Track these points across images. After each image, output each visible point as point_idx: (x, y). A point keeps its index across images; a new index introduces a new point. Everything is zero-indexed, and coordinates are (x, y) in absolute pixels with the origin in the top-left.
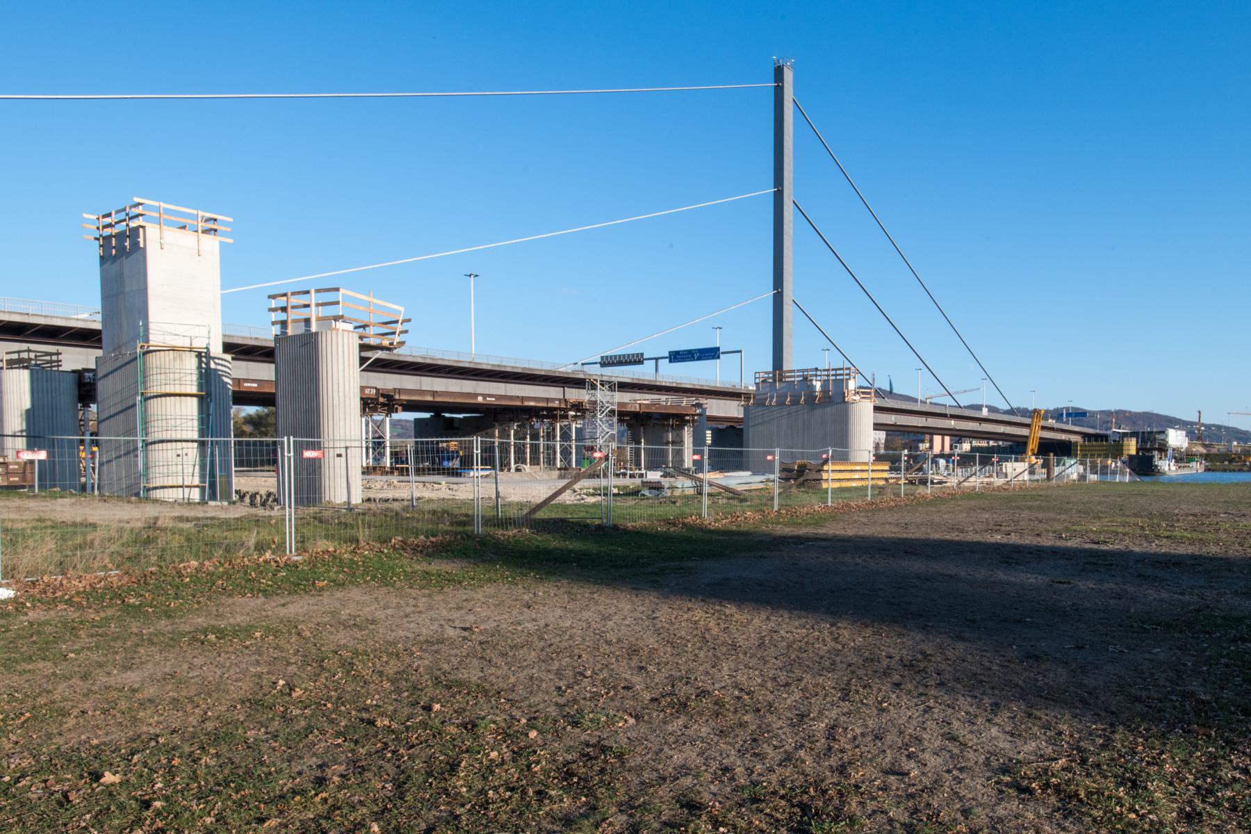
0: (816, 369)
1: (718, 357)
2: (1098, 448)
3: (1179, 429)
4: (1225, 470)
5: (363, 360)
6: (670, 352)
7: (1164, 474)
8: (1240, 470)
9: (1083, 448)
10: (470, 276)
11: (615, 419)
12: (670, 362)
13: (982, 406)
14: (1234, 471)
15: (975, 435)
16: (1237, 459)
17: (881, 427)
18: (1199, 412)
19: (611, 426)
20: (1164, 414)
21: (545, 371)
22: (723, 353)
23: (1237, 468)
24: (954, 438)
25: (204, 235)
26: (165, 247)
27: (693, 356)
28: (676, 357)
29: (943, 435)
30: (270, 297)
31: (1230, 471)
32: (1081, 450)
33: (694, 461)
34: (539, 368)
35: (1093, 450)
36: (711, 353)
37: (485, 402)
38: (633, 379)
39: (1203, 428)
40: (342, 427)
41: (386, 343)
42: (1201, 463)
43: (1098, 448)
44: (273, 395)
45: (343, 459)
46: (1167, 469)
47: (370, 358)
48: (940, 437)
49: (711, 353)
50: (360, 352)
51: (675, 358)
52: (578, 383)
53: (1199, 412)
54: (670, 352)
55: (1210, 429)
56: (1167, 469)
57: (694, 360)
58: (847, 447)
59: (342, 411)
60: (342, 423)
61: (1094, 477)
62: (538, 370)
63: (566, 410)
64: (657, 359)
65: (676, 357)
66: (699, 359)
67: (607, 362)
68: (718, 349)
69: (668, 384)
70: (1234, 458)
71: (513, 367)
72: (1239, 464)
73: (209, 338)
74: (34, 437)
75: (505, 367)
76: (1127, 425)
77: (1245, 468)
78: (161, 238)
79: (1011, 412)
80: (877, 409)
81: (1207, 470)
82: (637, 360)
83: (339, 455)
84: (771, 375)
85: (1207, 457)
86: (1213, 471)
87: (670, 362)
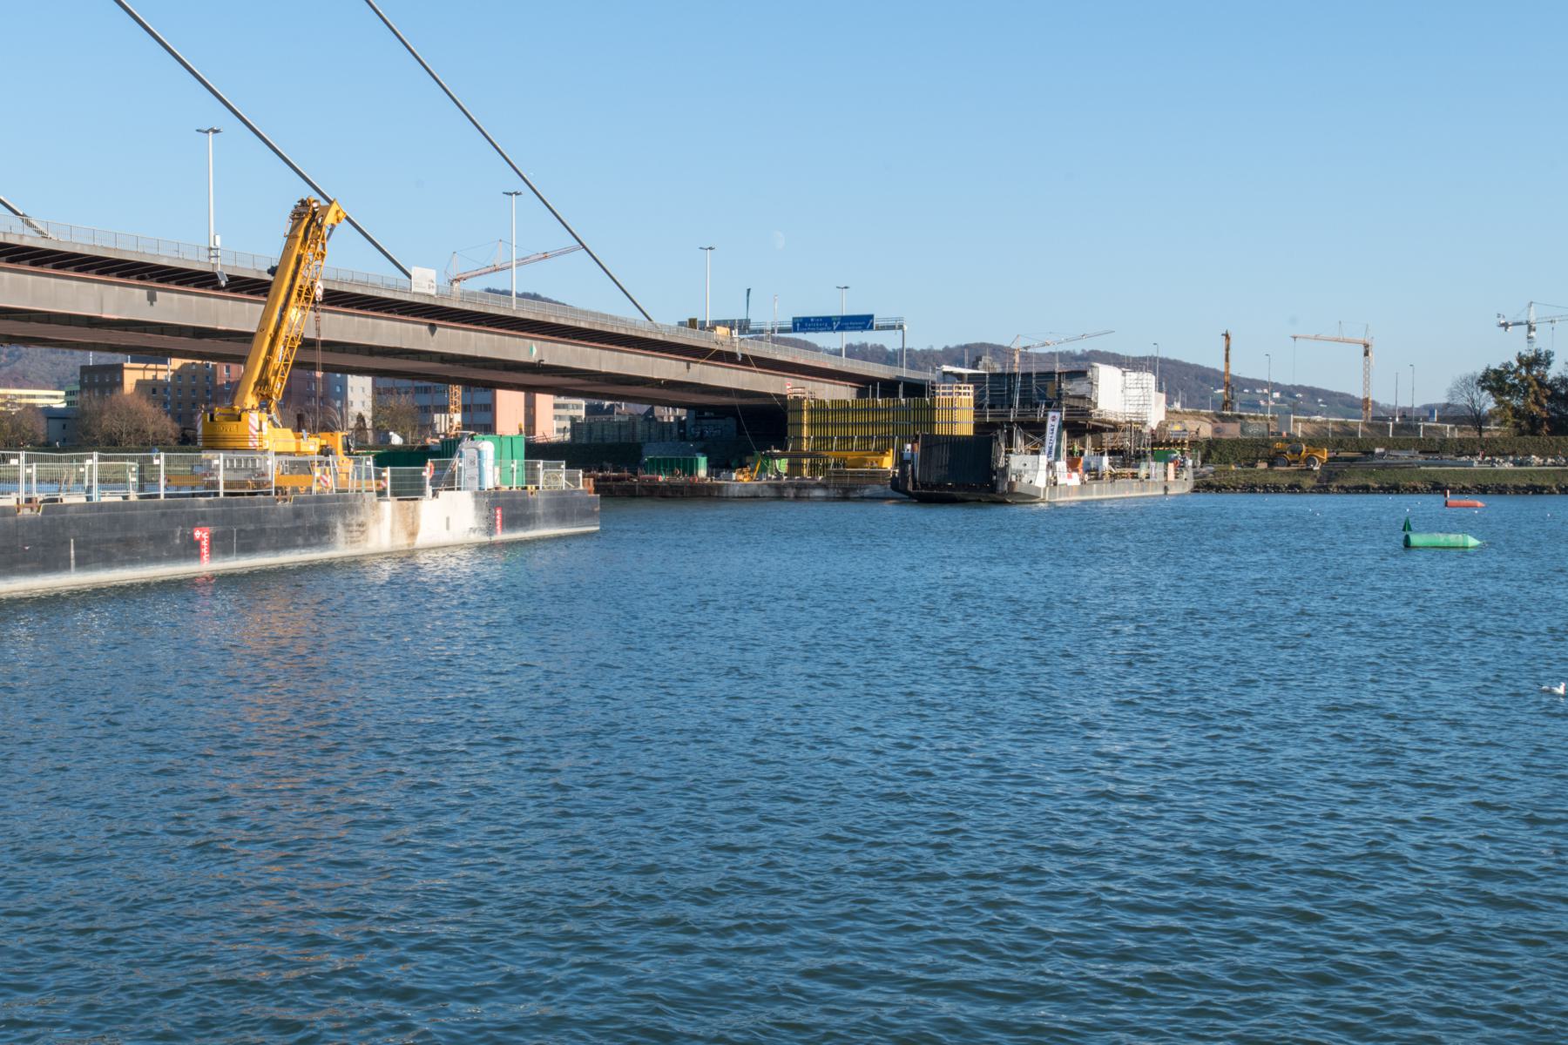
2: (861, 418)
4: (1251, 489)
7: (1029, 498)
8: (1294, 488)
9: (819, 418)
10: (207, 132)
14: (1277, 489)
16: (1289, 456)
18: (1227, 336)
20: (1192, 362)
23: (1287, 481)
24: (387, 382)
29: (530, 390)
31: (1266, 489)
32: (812, 425)
33: (1550, 433)
35: (846, 425)
39: (1277, 395)
42: (1180, 467)
43: (861, 418)
46: (1040, 481)
53: (1227, 336)
55: (1291, 395)
56: (1040, 481)
57: (832, 330)
70: (1281, 453)
72: (1293, 468)
77: (1308, 482)
81: (1203, 486)
85: (1210, 450)
86: (1219, 489)
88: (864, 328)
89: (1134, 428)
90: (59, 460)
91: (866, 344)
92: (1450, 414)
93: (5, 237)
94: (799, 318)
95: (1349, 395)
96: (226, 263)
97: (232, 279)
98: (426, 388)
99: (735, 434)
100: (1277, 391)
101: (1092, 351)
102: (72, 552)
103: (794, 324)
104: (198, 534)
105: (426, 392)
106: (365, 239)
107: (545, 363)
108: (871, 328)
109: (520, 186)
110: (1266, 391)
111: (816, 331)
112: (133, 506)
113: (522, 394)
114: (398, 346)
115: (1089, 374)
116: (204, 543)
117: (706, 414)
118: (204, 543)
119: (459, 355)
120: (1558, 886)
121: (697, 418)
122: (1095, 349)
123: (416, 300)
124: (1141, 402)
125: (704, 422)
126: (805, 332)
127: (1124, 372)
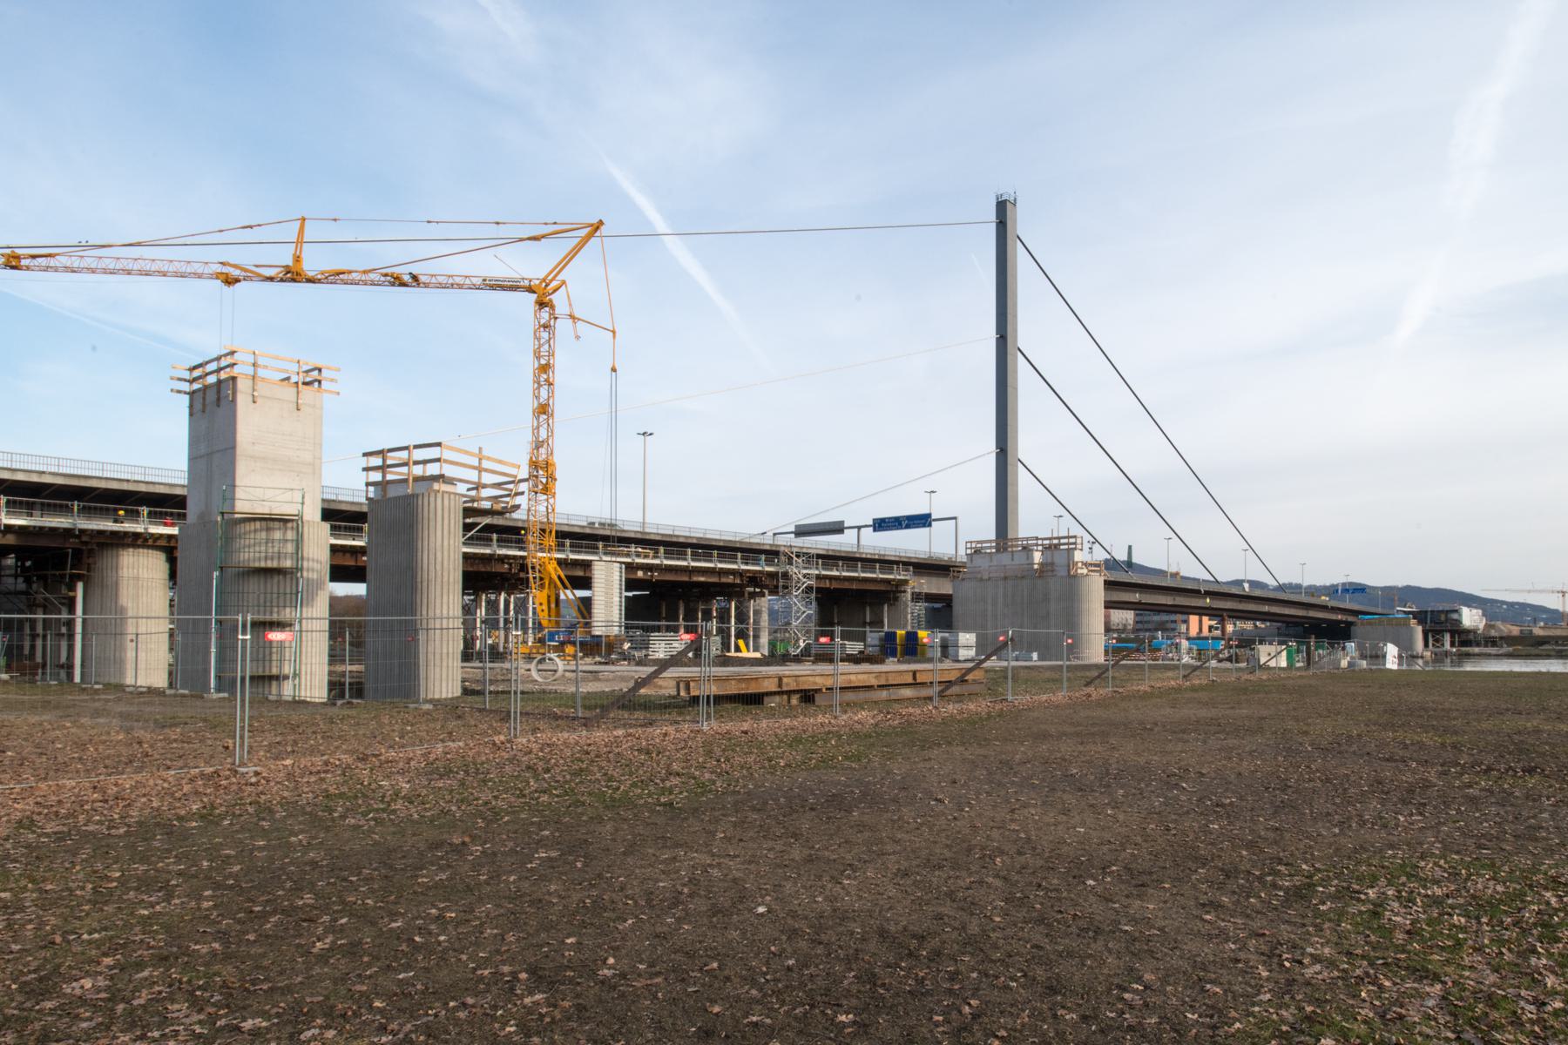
0: (1037, 539)
1: (930, 525)
3: (1476, 608)
5: (467, 527)
6: (874, 520)
11: (813, 596)
12: (875, 530)
13: (1243, 581)
15: (1115, 605)
17: (1130, 606)
19: (808, 604)
21: (724, 541)
22: (935, 520)
25: (305, 387)
26: (259, 401)
27: (900, 524)
28: (881, 525)
29: (1201, 615)
30: (365, 455)
34: (718, 537)
36: (923, 521)
37: (645, 577)
38: (828, 550)
40: (438, 605)
41: (498, 507)
44: (951, 596)
45: (134, 644)
47: (480, 524)
48: (1197, 617)
49: (923, 521)
50: (464, 518)
51: (880, 526)
52: (772, 554)
54: (874, 520)
58: (413, 612)
59: (438, 587)
60: (438, 601)
61: (1364, 664)
62: (716, 540)
63: (742, 586)
64: (859, 528)
65: (881, 525)
66: (908, 527)
67: (801, 531)
68: (929, 515)
69: (869, 556)
71: (686, 537)
73: (303, 504)
74: (312, 619)
75: (678, 536)
76: (1413, 603)
78: (254, 390)
79: (1281, 588)
80: (1109, 585)
82: (837, 528)
83: (132, 641)
84: (994, 544)
87: (875, 530)
89: (1474, 631)
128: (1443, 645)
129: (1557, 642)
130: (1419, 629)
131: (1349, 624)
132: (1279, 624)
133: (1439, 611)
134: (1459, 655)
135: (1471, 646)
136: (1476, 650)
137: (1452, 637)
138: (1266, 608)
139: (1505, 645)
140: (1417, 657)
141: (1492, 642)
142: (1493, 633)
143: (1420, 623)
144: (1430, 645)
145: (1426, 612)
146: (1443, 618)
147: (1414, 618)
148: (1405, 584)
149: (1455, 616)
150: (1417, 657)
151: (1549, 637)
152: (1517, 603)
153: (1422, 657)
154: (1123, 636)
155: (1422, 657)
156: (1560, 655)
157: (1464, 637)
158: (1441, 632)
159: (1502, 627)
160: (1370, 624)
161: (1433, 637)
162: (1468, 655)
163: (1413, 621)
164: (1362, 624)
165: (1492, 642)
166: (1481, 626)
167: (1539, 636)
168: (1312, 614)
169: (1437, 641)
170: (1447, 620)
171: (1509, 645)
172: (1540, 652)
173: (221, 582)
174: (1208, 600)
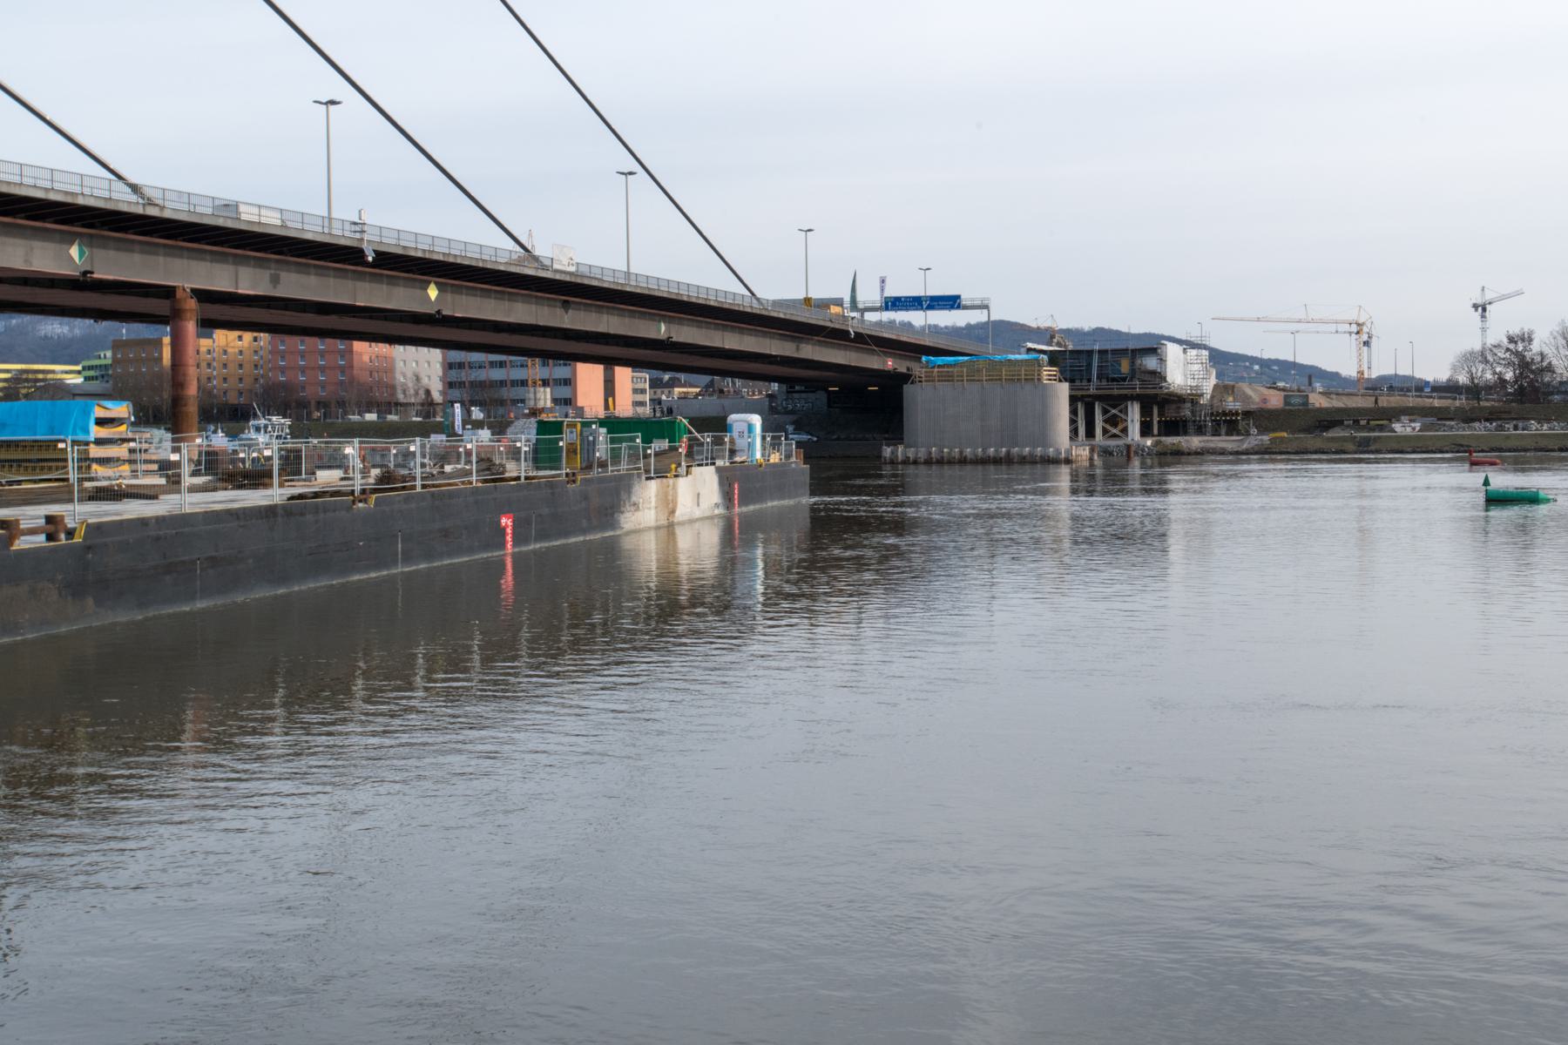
29: (609, 362)
55: (1269, 367)
57: (922, 309)
88: (952, 307)
89: (1192, 399)
90: (1377, 461)
91: (895, 321)
92: (1450, 389)
93: (144, 210)
94: (891, 298)
95: (1317, 368)
96: (371, 238)
97: (378, 254)
98: (501, 362)
99: (826, 408)
100: (1257, 364)
101: (1097, 328)
102: (400, 546)
103: (886, 303)
104: (504, 521)
105: (501, 367)
106: (672, 195)
107: (673, 340)
108: (959, 307)
109: (638, 168)
110: (1247, 364)
111: (907, 310)
112: (476, 491)
113: (601, 367)
114: (534, 323)
115: (1159, 351)
116: (509, 531)
117: (797, 388)
118: (509, 531)
119: (592, 332)
120: (723, 676)
121: (788, 392)
122: (1100, 326)
123: (558, 277)
124: (1202, 376)
125: (796, 395)
126: (896, 311)
127: (1185, 349)
128: (1125, 431)
129: (1356, 422)
130: (1063, 390)
131: (898, 381)
132: (775, 386)
133: (1115, 352)
134: (1161, 454)
135: (1186, 433)
136: (1195, 442)
137: (1146, 411)
138: (662, 330)
139: (1254, 431)
140: (1056, 461)
141: (1228, 423)
142: (1231, 404)
143: (1069, 376)
144: (1098, 431)
145: (1090, 353)
146: (1125, 367)
147: (1052, 362)
148: (1094, 326)
149: (1151, 363)
150: (1056, 461)
151: (1339, 410)
152: (1277, 362)
153: (1068, 461)
154: (392, 418)
155: (1068, 461)
156: (2, 441)
157: (1171, 414)
158: (1119, 401)
159: (1249, 392)
160: (948, 378)
161: (1105, 412)
162: (1178, 455)
163: (1048, 372)
164: (930, 379)
165: (1228, 423)
166: (1208, 386)
167: (1320, 410)
168: (810, 351)
169: (1113, 421)
170: (1133, 371)
171: (1263, 430)
172: (1325, 446)
173: (635, 422)
174: (433, 292)
